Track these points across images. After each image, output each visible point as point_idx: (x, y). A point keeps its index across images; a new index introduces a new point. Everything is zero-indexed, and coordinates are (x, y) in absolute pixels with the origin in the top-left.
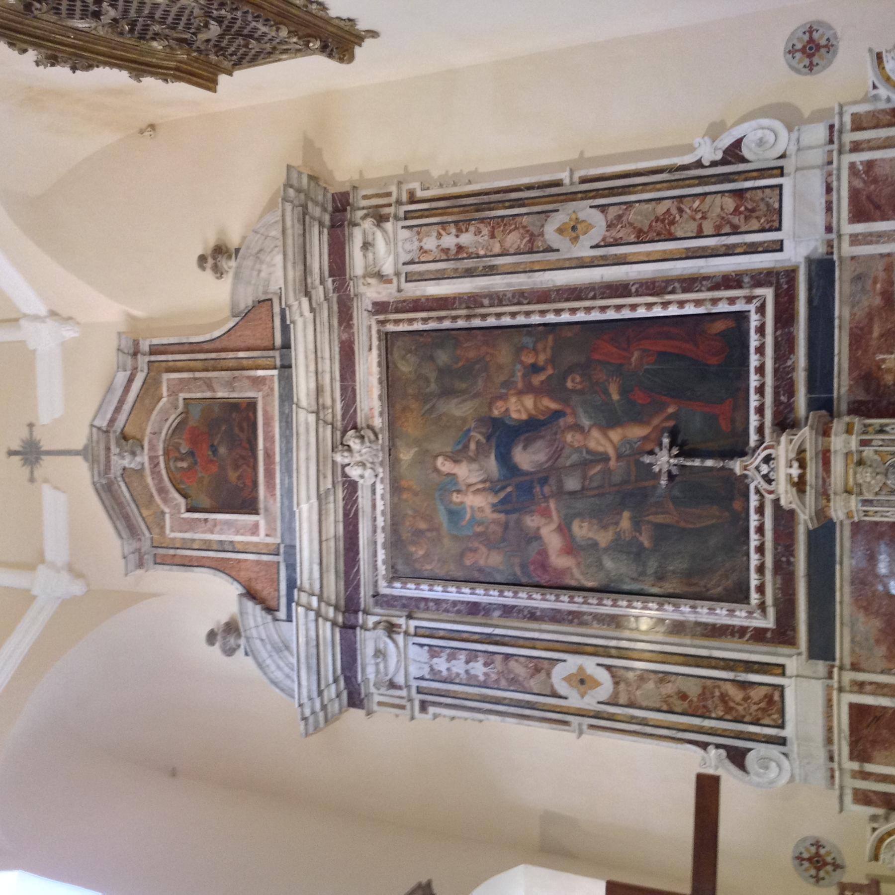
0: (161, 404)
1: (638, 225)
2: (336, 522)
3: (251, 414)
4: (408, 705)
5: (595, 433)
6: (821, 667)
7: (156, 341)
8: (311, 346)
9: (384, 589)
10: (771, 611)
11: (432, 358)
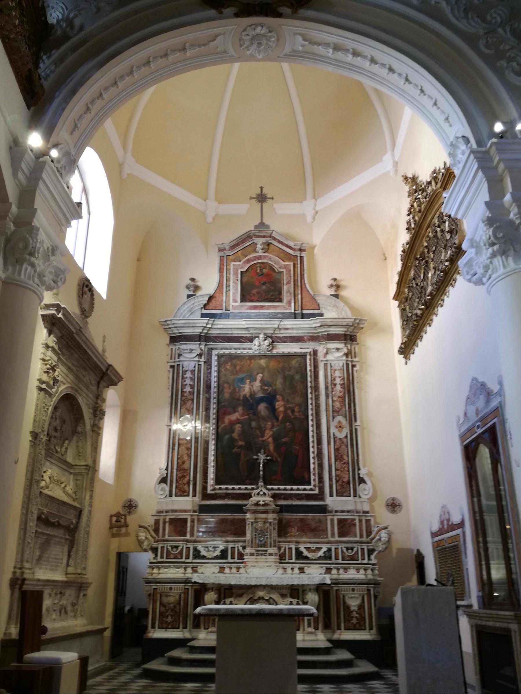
0: (282, 262)
1: (340, 449)
2: (238, 334)
3: (277, 300)
4: (172, 361)
5: (271, 433)
6: (197, 508)
7: (305, 259)
8: (302, 326)
9: (215, 352)
10: (213, 492)
11: (297, 373)
